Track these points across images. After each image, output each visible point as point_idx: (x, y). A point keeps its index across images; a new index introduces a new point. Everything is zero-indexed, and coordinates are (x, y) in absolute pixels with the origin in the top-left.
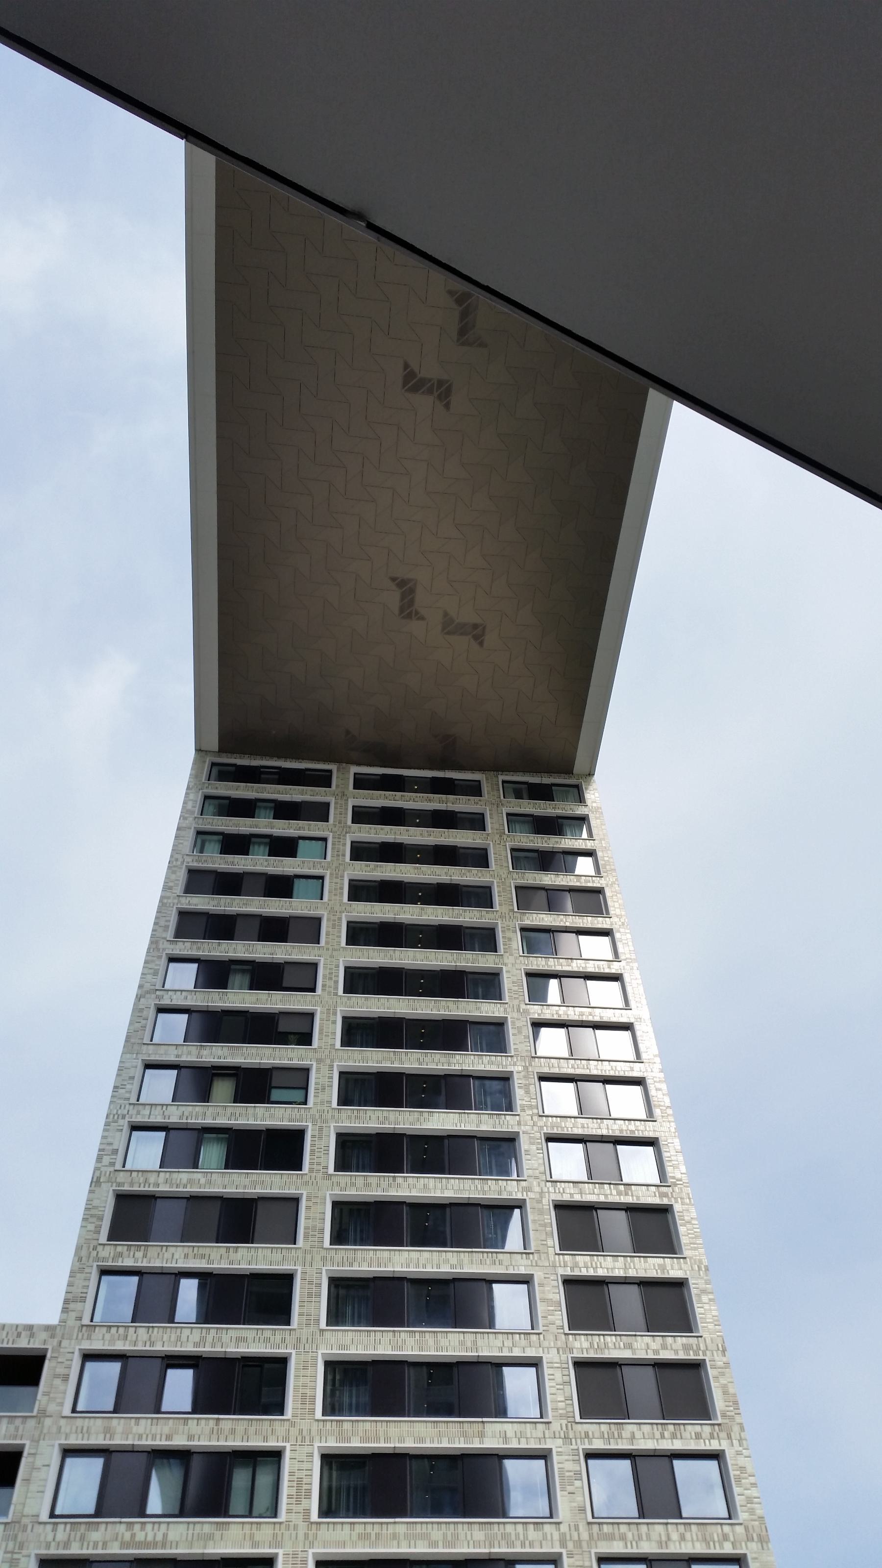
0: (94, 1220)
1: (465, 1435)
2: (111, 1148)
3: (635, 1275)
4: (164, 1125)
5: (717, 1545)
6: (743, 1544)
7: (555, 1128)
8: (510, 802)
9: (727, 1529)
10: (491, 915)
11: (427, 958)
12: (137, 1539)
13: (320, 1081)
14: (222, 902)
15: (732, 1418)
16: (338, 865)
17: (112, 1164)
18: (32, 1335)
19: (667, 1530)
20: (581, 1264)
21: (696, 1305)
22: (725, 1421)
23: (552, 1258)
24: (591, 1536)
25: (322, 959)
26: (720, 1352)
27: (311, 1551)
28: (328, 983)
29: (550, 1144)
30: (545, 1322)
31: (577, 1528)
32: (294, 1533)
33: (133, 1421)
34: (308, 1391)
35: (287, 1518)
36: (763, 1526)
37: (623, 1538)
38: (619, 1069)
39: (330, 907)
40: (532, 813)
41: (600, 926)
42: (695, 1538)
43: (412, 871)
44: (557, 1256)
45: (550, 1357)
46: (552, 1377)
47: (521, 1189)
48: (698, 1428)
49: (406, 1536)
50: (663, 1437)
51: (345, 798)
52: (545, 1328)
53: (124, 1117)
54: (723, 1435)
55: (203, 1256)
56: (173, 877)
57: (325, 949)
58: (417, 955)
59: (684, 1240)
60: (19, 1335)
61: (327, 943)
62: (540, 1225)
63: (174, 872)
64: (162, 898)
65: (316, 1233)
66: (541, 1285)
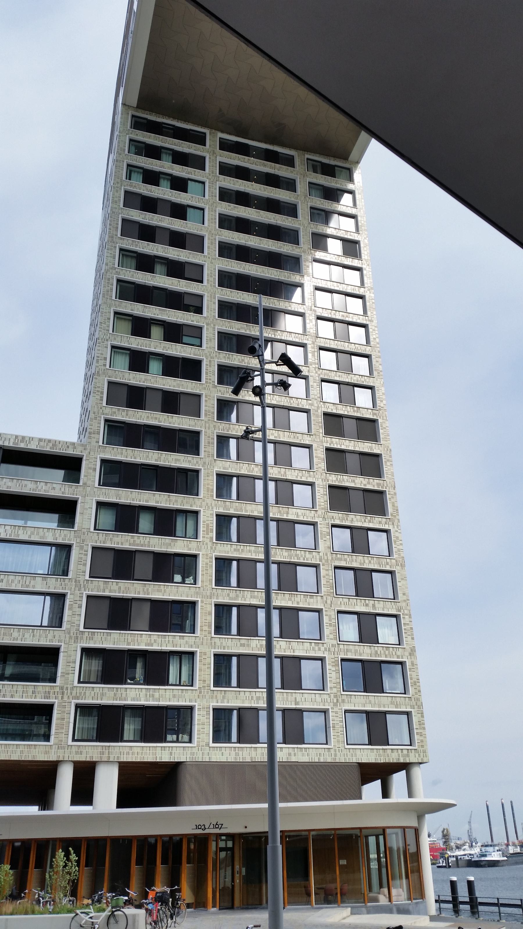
1: (280, 512)
5: (384, 566)
6: (394, 567)
7: (326, 376)
8: (310, 174)
9: (388, 560)
10: (298, 250)
13: (209, 335)
14: (147, 217)
15: (395, 516)
16: (212, 203)
17: (105, 365)
18: (75, 448)
20: (335, 442)
21: (384, 466)
22: (392, 517)
23: (321, 438)
24: (332, 558)
25: (206, 263)
27: (214, 554)
28: (210, 279)
29: (322, 383)
30: (317, 467)
31: (327, 554)
34: (210, 487)
36: (403, 561)
37: (345, 560)
38: (359, 348)
39: (209, 230)
40: (323, 184)
41: (348, 212)
42: (375, 563)
43: (255, 213)
45: (319, 482)
46: (319, 491)
47: (308, 404)
48: (380, 519)
49: (255, 552)
50: (365, 521)
51: (215, 155)
52: (317, 470)
53: (107, 340)
54: (391, 523)
55: (156, 418)
57: (208, 257)
58: (258, 269)
59: (382, 436)
60: (68, 447)
61: (208, 254)
62: (317, 422)
65: (211, 414)
66: (316, 450)
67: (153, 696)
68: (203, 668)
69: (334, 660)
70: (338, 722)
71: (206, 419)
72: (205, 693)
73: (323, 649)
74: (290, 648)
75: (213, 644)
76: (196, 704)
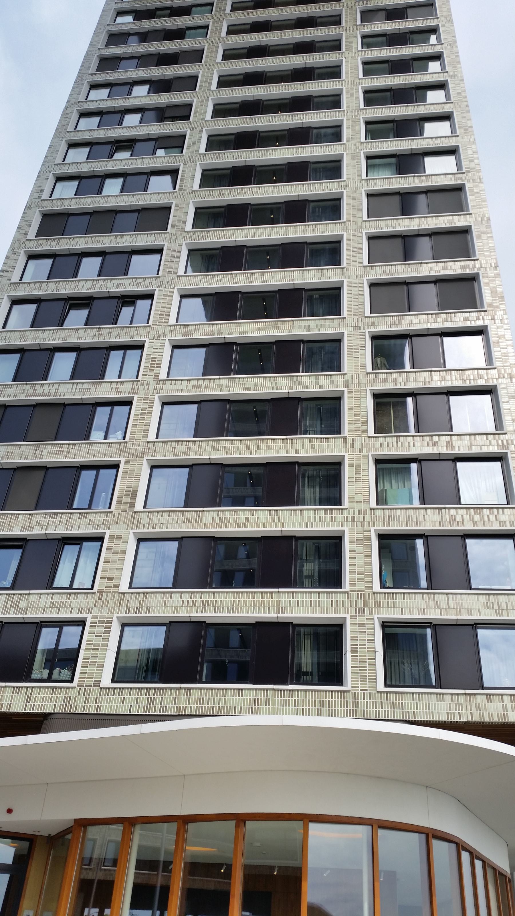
0: (25, 228)
1: (278, 328)
2: (40, 189)
3: (427, 227)
4: (78, 174)
11: (282, 61)
12: (37, 392)
19: (431, 375)
23: (359, 224)
26: (492, 268)
28: (204, 84)
31: (358, 377)
32: (147, 387)
33: (41, 332)
35: (78, 684)
39: (210, 41)
44: (364, 223)
48: (467, 315)
56: (97, 39)
59: (470, 204)
63: (97, 36)
64: (87, 52)
67: (17, 606)
68: (113, 558)
69: (361, 536)
70: (363, 642)
71: (173, 231)
72: (109, 598)
73: (339, 518)
74: (277, 520)
75: (136, 522)
76: (367, 331)
